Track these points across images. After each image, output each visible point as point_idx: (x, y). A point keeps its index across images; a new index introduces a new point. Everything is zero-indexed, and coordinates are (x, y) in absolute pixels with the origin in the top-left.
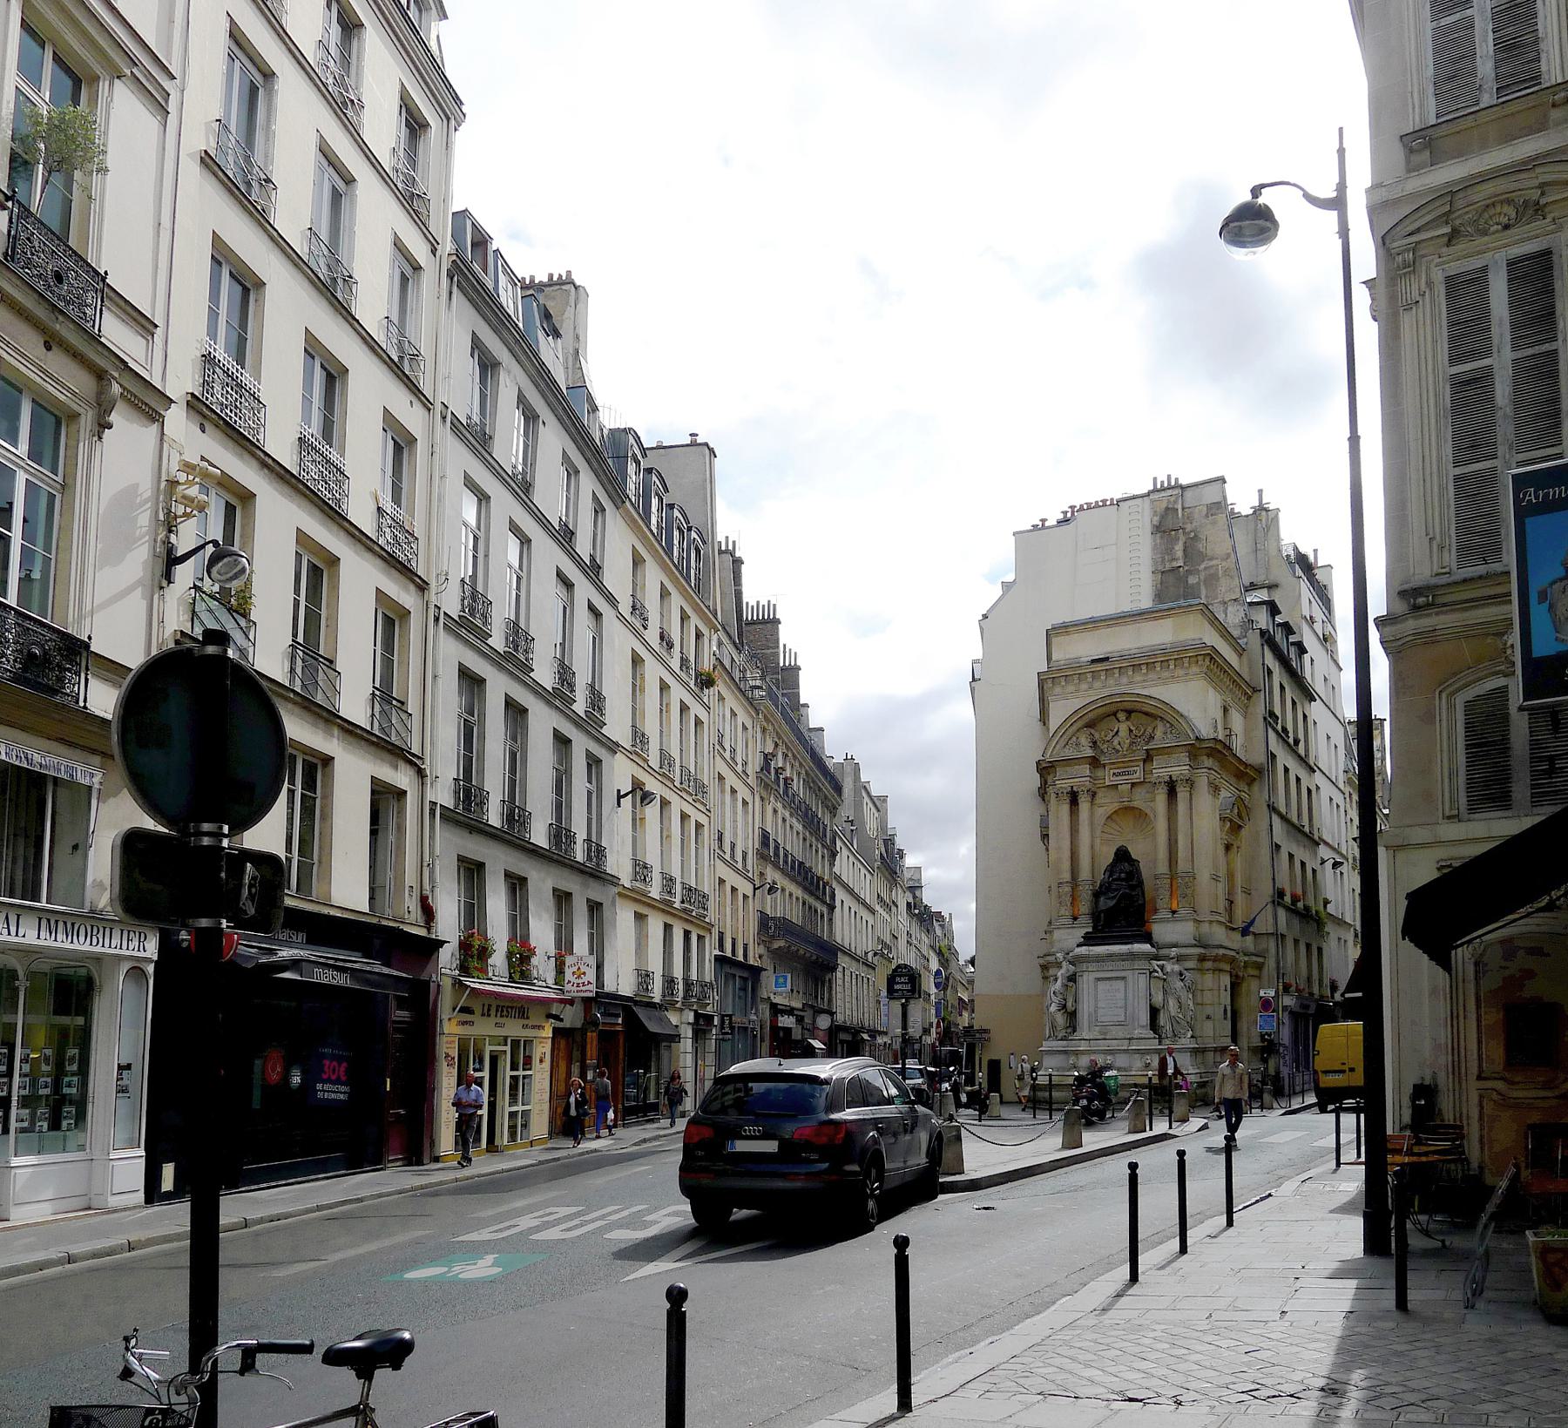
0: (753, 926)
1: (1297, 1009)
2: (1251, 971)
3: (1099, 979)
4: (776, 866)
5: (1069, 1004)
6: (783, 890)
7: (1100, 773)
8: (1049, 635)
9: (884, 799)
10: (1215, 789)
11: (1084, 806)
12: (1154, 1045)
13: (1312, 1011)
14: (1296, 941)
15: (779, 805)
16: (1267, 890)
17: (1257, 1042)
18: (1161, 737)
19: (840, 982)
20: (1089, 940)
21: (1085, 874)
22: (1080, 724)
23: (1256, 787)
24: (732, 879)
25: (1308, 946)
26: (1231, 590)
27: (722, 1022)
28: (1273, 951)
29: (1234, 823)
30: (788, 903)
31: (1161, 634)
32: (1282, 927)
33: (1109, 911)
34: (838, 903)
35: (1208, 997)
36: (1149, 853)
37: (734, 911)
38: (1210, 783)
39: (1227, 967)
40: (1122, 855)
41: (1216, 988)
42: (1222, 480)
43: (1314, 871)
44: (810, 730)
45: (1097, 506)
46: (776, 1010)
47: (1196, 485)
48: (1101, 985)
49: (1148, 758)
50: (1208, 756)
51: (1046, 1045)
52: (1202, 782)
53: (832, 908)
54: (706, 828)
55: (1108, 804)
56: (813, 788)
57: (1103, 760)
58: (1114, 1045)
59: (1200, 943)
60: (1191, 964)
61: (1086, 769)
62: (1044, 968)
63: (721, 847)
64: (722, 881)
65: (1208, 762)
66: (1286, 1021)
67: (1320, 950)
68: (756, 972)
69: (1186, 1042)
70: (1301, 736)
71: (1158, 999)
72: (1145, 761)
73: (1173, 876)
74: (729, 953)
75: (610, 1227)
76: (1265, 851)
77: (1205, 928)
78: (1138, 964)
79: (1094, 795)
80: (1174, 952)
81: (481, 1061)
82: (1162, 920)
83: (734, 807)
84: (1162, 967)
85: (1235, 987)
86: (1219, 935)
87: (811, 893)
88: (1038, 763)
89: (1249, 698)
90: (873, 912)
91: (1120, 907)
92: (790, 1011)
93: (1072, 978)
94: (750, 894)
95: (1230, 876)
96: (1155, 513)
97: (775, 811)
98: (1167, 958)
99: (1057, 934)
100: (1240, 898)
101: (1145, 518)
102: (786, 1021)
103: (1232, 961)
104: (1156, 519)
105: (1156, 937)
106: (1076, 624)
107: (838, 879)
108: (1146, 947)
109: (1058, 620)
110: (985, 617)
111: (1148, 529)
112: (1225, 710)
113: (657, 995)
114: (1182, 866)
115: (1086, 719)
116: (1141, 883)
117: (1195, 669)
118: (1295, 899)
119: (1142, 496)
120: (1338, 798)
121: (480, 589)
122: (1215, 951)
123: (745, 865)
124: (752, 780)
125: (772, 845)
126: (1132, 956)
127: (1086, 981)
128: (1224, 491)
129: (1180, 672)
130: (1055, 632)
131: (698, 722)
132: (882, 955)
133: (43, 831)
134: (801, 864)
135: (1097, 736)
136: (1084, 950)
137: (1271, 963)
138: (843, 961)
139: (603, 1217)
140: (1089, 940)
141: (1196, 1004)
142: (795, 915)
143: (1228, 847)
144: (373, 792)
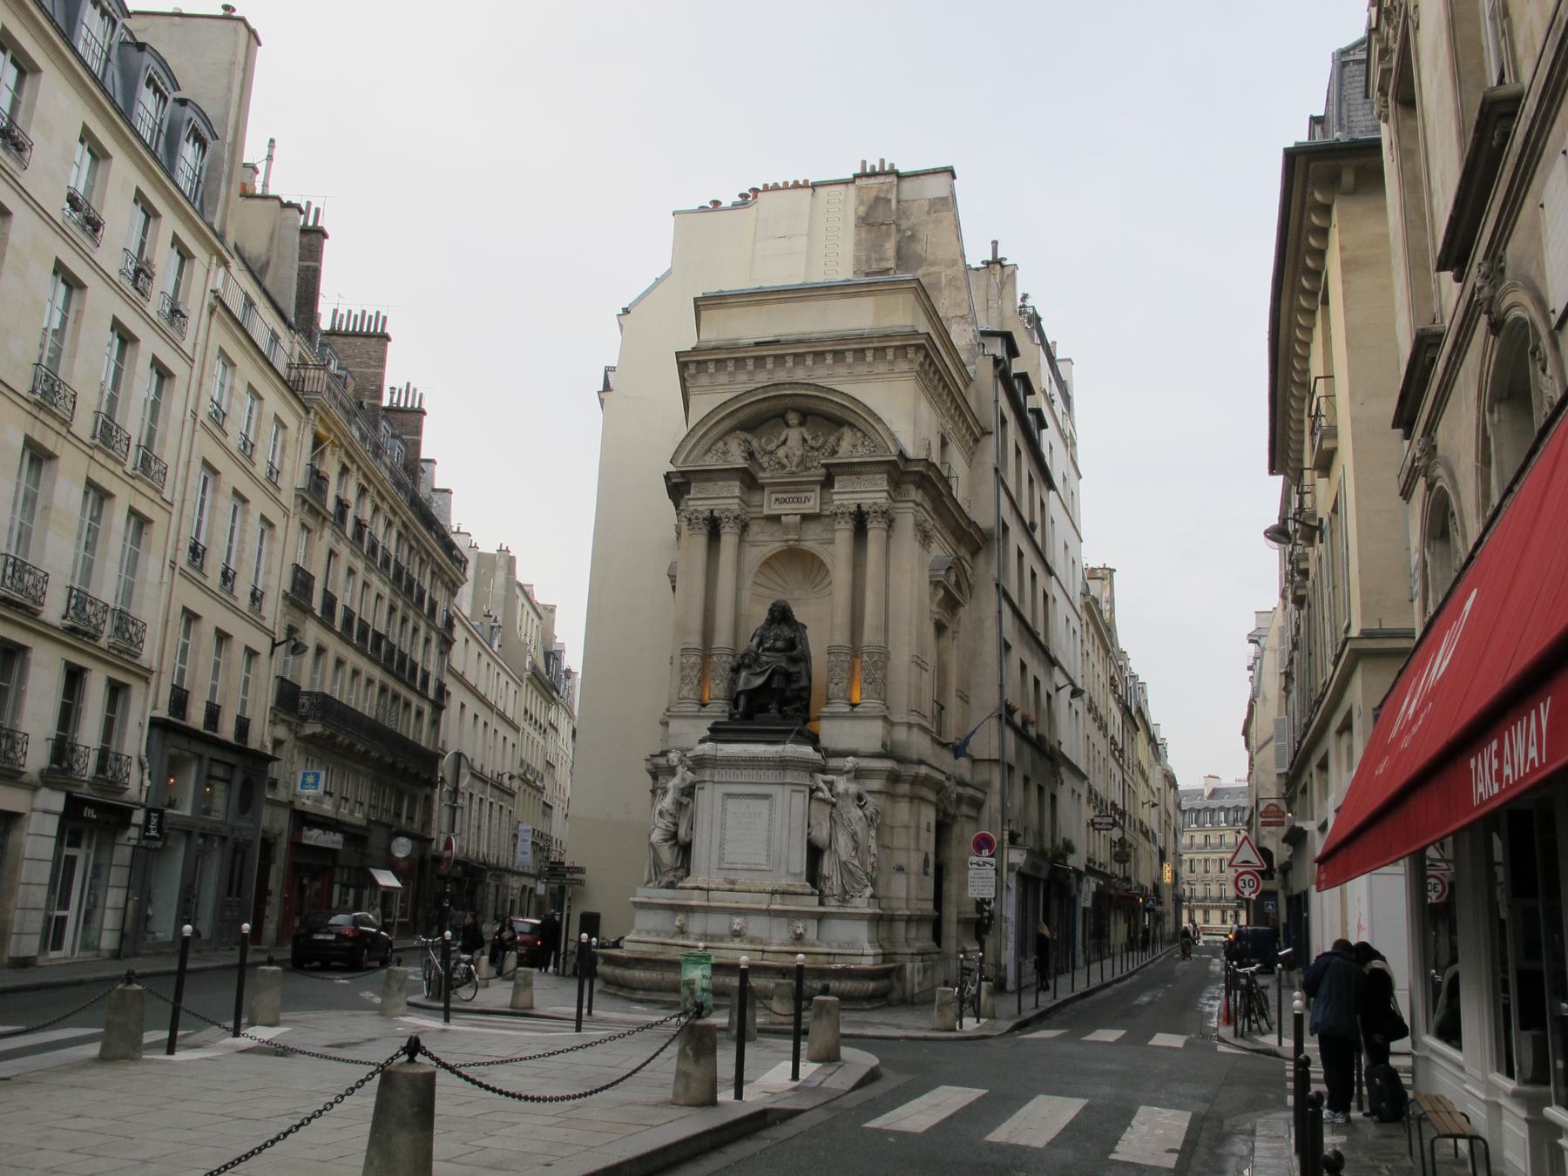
1: (1027, 871)
2: (965, 809)
3: (729, 795)
5: (682, 833)
6: (320, 650)
7: (756, 498)
9: (551, 610)
10: (925, 538)
11: (728, 539)
12: (811, 904)
13: (1044, 875)
14: (1026, 780)
16: (991, 700)
17: (970, 912)
18: (848, 448)
20: (718, 733)
21: (723, 639)
22: (727, 424)
23: (981, 559)
25: (1041, 789)
26: (958, 305)
27: (148, 820)
28: (997, 783)
29: (951, 597)
31: (857, 316)
32: (1010, 755)
33: (752, 694)
35: (901, 839)
36: (822, 622)
39: (932, 796)
40: (781, 615)
41: (913, 824)
42: (950, 172)
43: (1049, 696)
44: (434, 490)
45: (786, 187)
46: (303, 819)
47: (916, 175)
48: (732, 804)
49: (827, 483)
50: (918, 486)
51: (643, 894)
52: (906, 521)
55: (766, 543)
56: (420, 545)
57: (763, 477)
58: (746, 901)
59: (887, 753)
60: (876, 784)
61: (735, 488)
62: (655, 774)
64: (191, 617)
65: (915, 494)
66: (1013, 885)
67: (1054, 798)
69: (862, 904)
70: (1038, 520)
71: (822, 834)
73: (855, 649)
76: (990, 648)
77: (901, 734)
78: (790, 777)
79: (744, 527)
80: (850, 762)
82: (834, 716)
84: (831, 785)
85: (942, 829)
86: (920, 744)
88: (667, 477)
89: (976, 441)
90: (517, 729)
91: (769, 694)
92: (327, 824)
93: (689, 791)
95: (942, 671)
96: (861, 203)
98: (839, 772)
99: (675, 725)
100: (953, 703)
101: (847, 205)
103: (939, 788)
104: (862, 210)
105: (825, 741)
107: (460, 678)
108: (807, 751)
109: (713, 289)
110: (626, 311)
111: (852, 221)
112: (944, 444)
114: (870, 636)
115: (742, 415)
116: (805, 658)
117: (902, 366)
118: (1025, 722)
119: (845, 182)
120: (1074, 622)
121: (251, 438)
122: (913, 770)
126: (783, 764)
127: (708, 799)
128: (952, 187)
129: (882, 368)
130: (702, 304)
131: (163, 373)
132: (526, 782)
133: (1074, 931)
134: (378, 637)
135: (755, 443)
136: (708, 748)
137: (993, 802)
140: (718, 733)
141: (882, 847)
143: (940, 628)
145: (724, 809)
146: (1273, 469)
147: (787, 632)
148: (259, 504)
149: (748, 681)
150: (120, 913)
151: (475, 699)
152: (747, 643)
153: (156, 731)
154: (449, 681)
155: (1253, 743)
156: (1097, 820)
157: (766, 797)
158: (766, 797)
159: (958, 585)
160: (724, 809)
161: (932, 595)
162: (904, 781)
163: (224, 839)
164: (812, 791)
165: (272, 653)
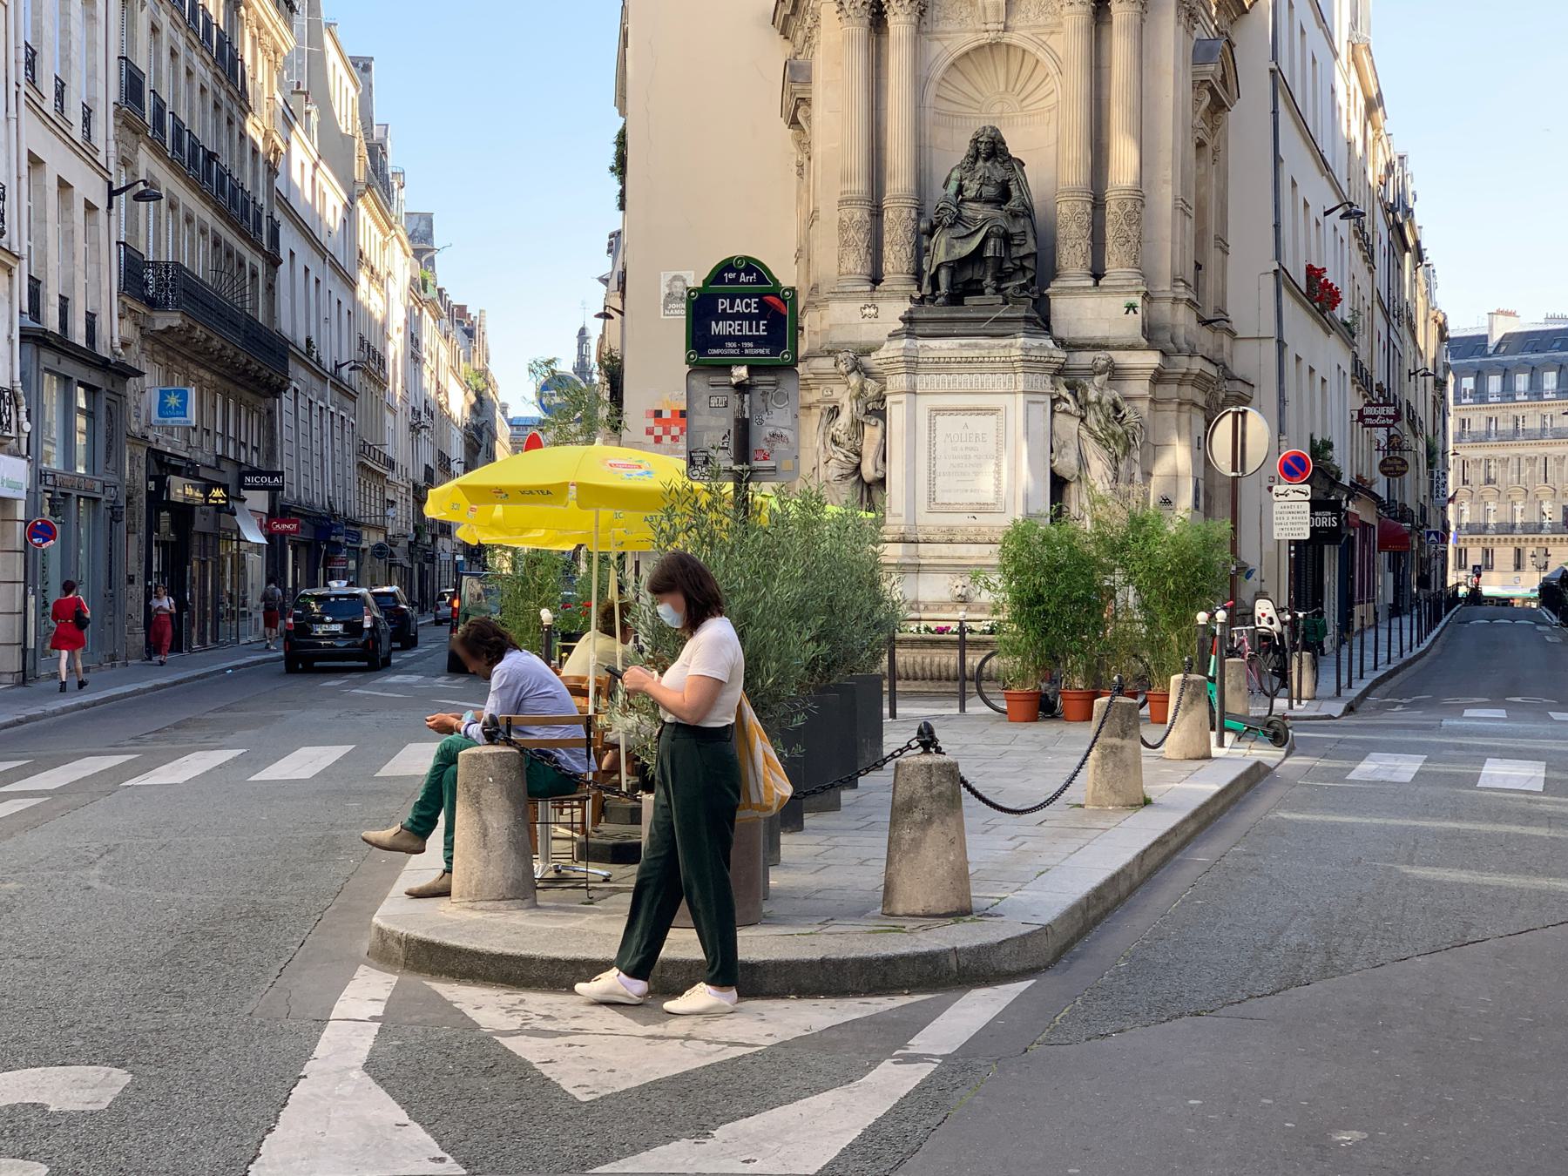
4: (157, 149)
21: (899, 182)
71: (1067, 464)
125: (169, 119)
134: (211, 157)
143: (1200, 145)
145: (932, 428)
149: (950, 247)
150: (18, 618)
151: (308, 248)
152: (940, 194)
153: (29, 347)
154: (278, 215)
156: (1368, 411)
157: (993, 411)
158: (993, 411)
159: (1224, 81)
160: (932, 428)
161: (1197, 101)
162: (1170, 382)
164: (1054, 402)
165: (110, 206)
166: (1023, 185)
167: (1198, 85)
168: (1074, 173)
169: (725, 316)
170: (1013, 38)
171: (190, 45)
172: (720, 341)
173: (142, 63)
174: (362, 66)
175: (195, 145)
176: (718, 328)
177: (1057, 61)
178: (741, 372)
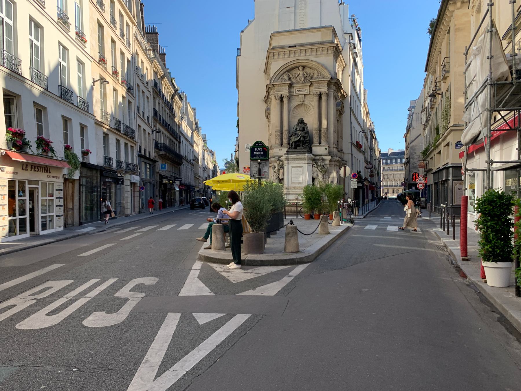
0: (153, 146)
3: (292, 167)
4: (160, 124)
8: (271, 36)
15: (161, 102)
19: (183, 169)
21: (286, 127)
24: (144, 126)
30: (164, 138)
34: (181, 141)
37: (145, 139)
38: (334, 96)
46: (162, 177)
53: (180, 143)
54: (133, 104)
63: (139, 112)
68: (155, 161)
71: (315, 175)
72: (310, 86)
74: (143, 153)
75: (85, 311)
81: (24, 191)
82: (315, 146)
83: (144, 98)
87: (173, 136)
94: (151, 133)
97: (159, 103)
102: (165, 181)
106: (282, 32)
113: (114, 165)
123: (148, 122)
124: (151, 90)
125: (158, 115)
134: (169, 125)
135: (291, 76)
138: (184, 162)
139: (82, 294)
140: (288, 152)
142: (167, 143)
143: (338, 121)
144: (4, 95)
145: (291, 170)
146: (425, 71)
147: (303, 126)
148: (147, 93)
152: (293, 130)
155: (408, 141)
160: (291, 170)
161: (337, 113)
163: (151, 183)
166: (307, 128)
167: (337, 110)
168: (316, 126)
169: (256, 151)
170: (305, 103)
171: (165, 106)
172: (256, 155)
173: (157, 109)
174: (194, 109)
175: (166, 123)
176: (255, 153)
177: (313, 106)
178: (259, 161)
